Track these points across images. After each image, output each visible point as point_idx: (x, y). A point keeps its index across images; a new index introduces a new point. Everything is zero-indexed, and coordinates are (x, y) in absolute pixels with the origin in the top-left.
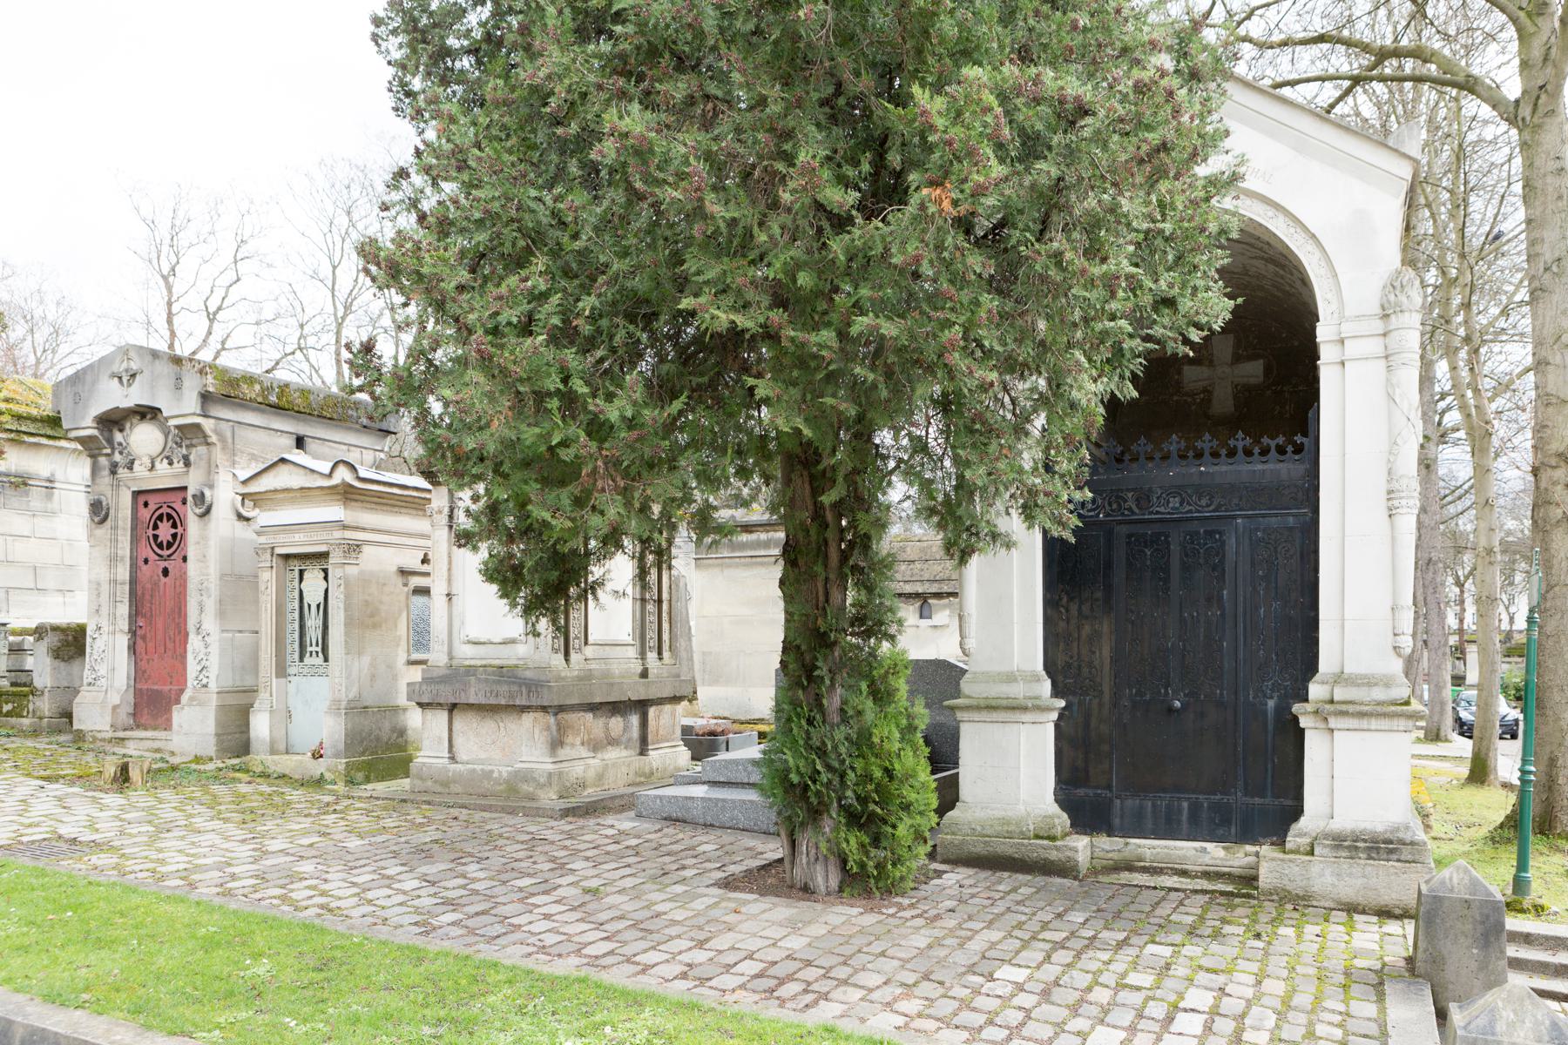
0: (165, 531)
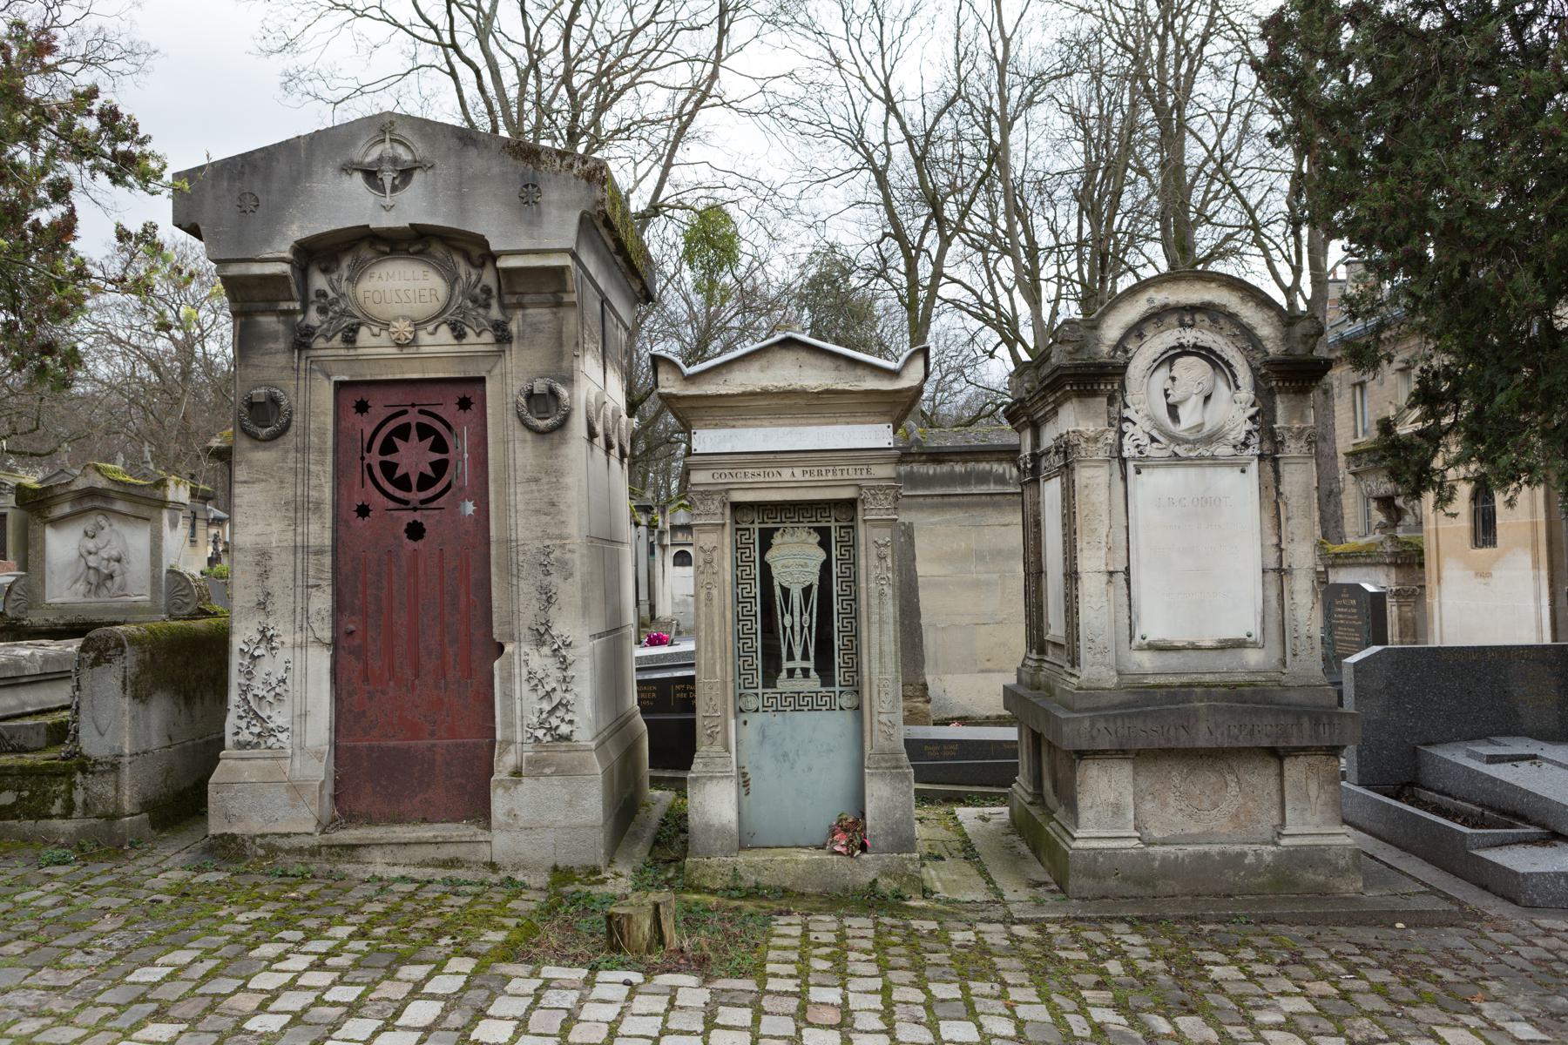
0: (413, 457)
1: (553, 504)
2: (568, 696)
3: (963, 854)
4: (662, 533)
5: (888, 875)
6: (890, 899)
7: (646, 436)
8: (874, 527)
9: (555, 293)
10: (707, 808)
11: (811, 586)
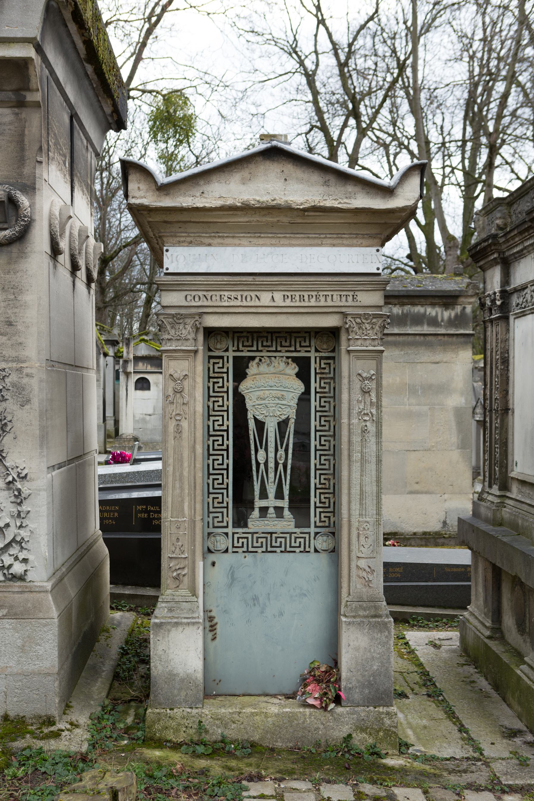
1: (10, 324)
2: (23, 533)
3: (424, 691)
4: (126, 362)
5: (363, 730)
6: (366, 756)
7: (115, 288)
8: (358, 358)
9: (17, 91)
10: (171, 656)
11: (288, 419)
